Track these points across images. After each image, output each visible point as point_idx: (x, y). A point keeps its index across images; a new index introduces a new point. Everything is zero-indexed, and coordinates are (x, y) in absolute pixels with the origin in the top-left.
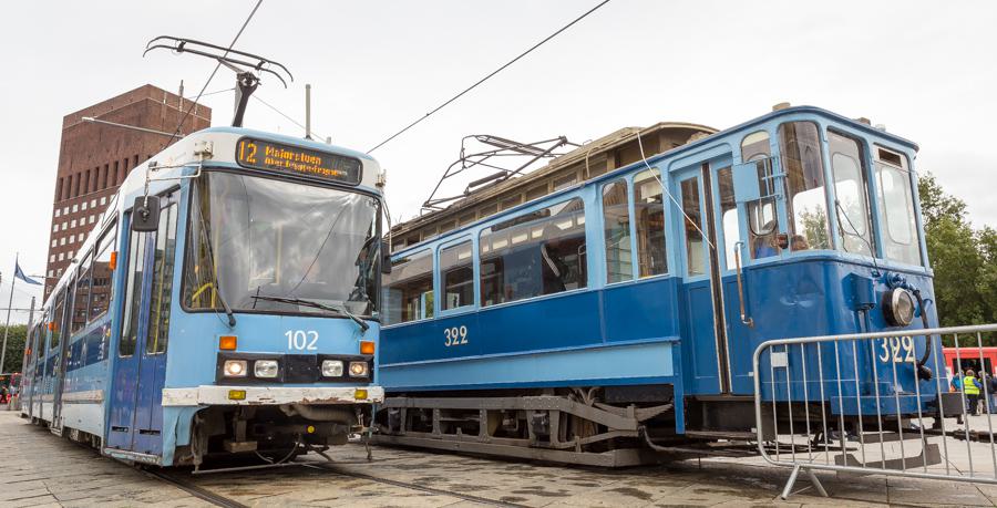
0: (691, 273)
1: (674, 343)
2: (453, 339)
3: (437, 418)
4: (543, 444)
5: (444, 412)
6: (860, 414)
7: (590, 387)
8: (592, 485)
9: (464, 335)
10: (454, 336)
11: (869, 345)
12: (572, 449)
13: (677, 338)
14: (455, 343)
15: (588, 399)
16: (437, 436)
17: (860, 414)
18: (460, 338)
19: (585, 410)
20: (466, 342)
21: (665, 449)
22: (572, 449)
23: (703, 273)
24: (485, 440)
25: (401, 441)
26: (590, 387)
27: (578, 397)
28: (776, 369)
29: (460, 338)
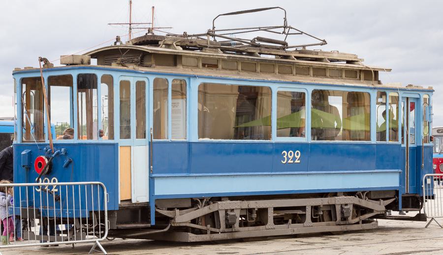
0: (121, 146)
1: (400, 172)
2: (288, 159)
3: (271, 215)
4: (230, 230)
5: (276, 209)
6: (55, 217)
7: (365, 192)
8: (359, 240)
9: (298, 157)
10: (289, 156)
11: (19, 188)
12: (358, 223)
13: (400, 171)
14: (290, 161)
15: (364, 196)
16: (271, 227)
17: (55, 217)
18: (294, 159)
19: (365, 203)
20: (299, 161)
21: (162, 231)
22: (358, 223)
23: (404, 145)
24: (271, 227)
25: (237, 236)
26: (365, 192)
27: (360, 197)
28: (428, 184)
29: (294, 159)
